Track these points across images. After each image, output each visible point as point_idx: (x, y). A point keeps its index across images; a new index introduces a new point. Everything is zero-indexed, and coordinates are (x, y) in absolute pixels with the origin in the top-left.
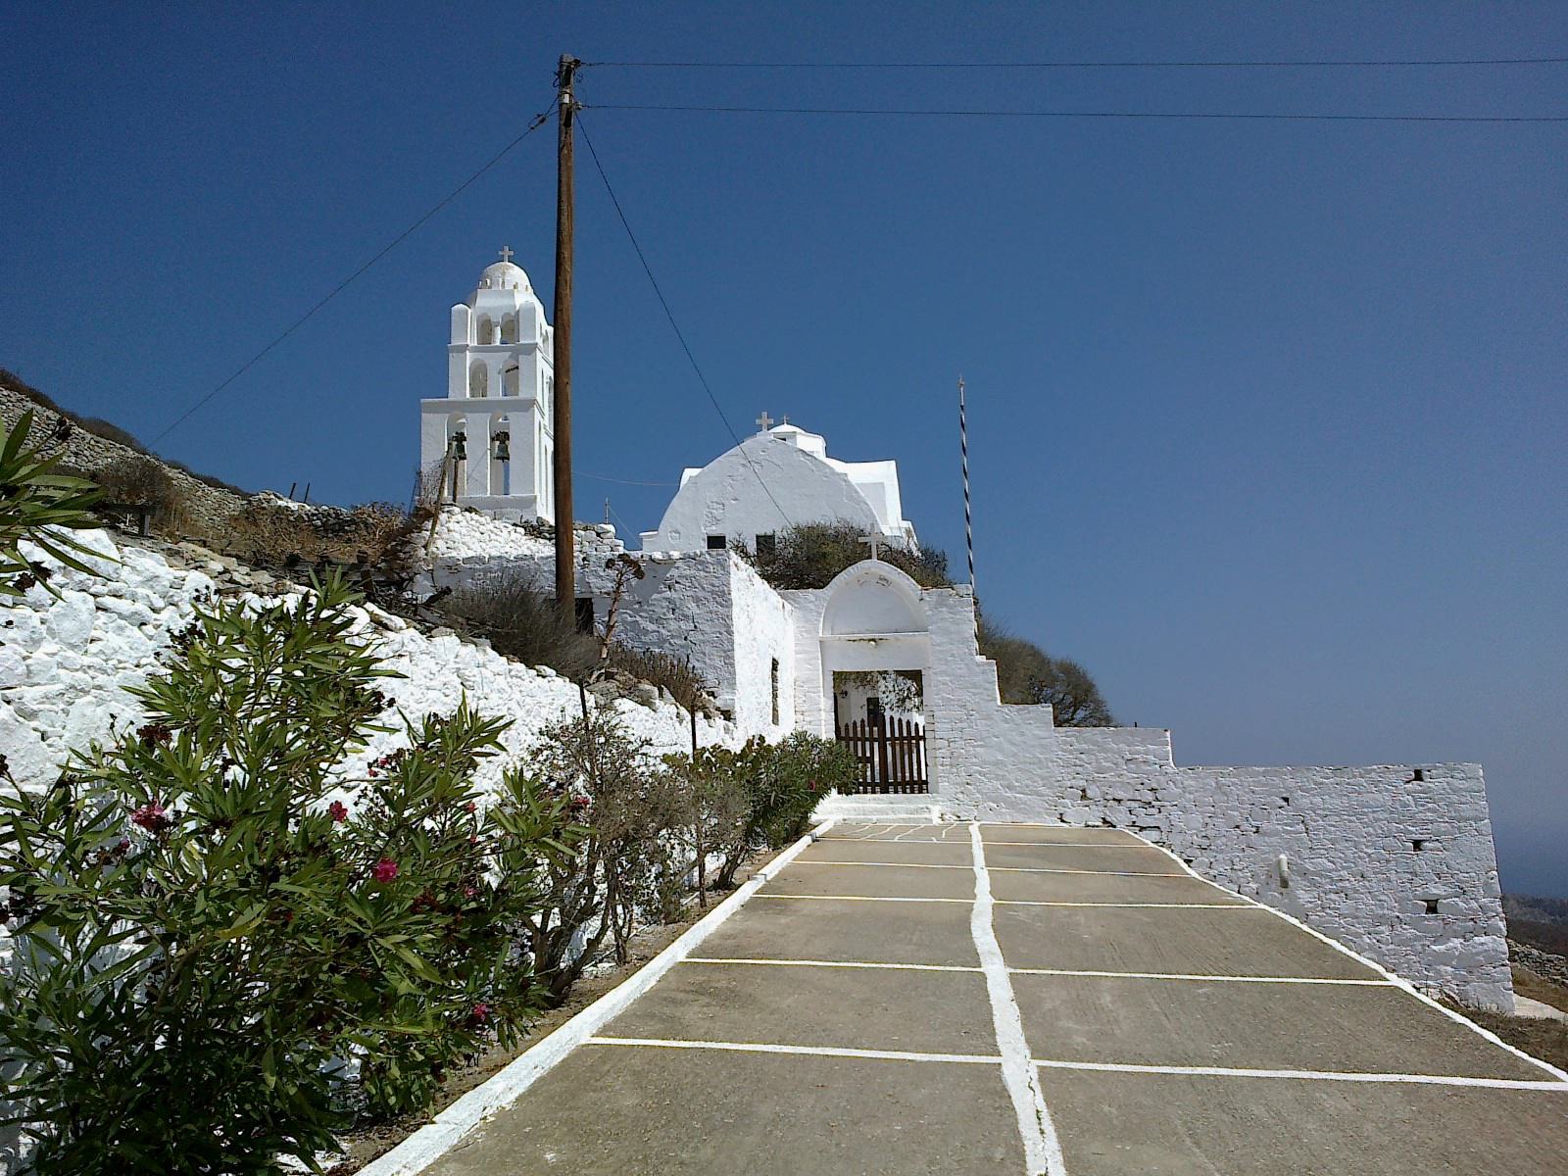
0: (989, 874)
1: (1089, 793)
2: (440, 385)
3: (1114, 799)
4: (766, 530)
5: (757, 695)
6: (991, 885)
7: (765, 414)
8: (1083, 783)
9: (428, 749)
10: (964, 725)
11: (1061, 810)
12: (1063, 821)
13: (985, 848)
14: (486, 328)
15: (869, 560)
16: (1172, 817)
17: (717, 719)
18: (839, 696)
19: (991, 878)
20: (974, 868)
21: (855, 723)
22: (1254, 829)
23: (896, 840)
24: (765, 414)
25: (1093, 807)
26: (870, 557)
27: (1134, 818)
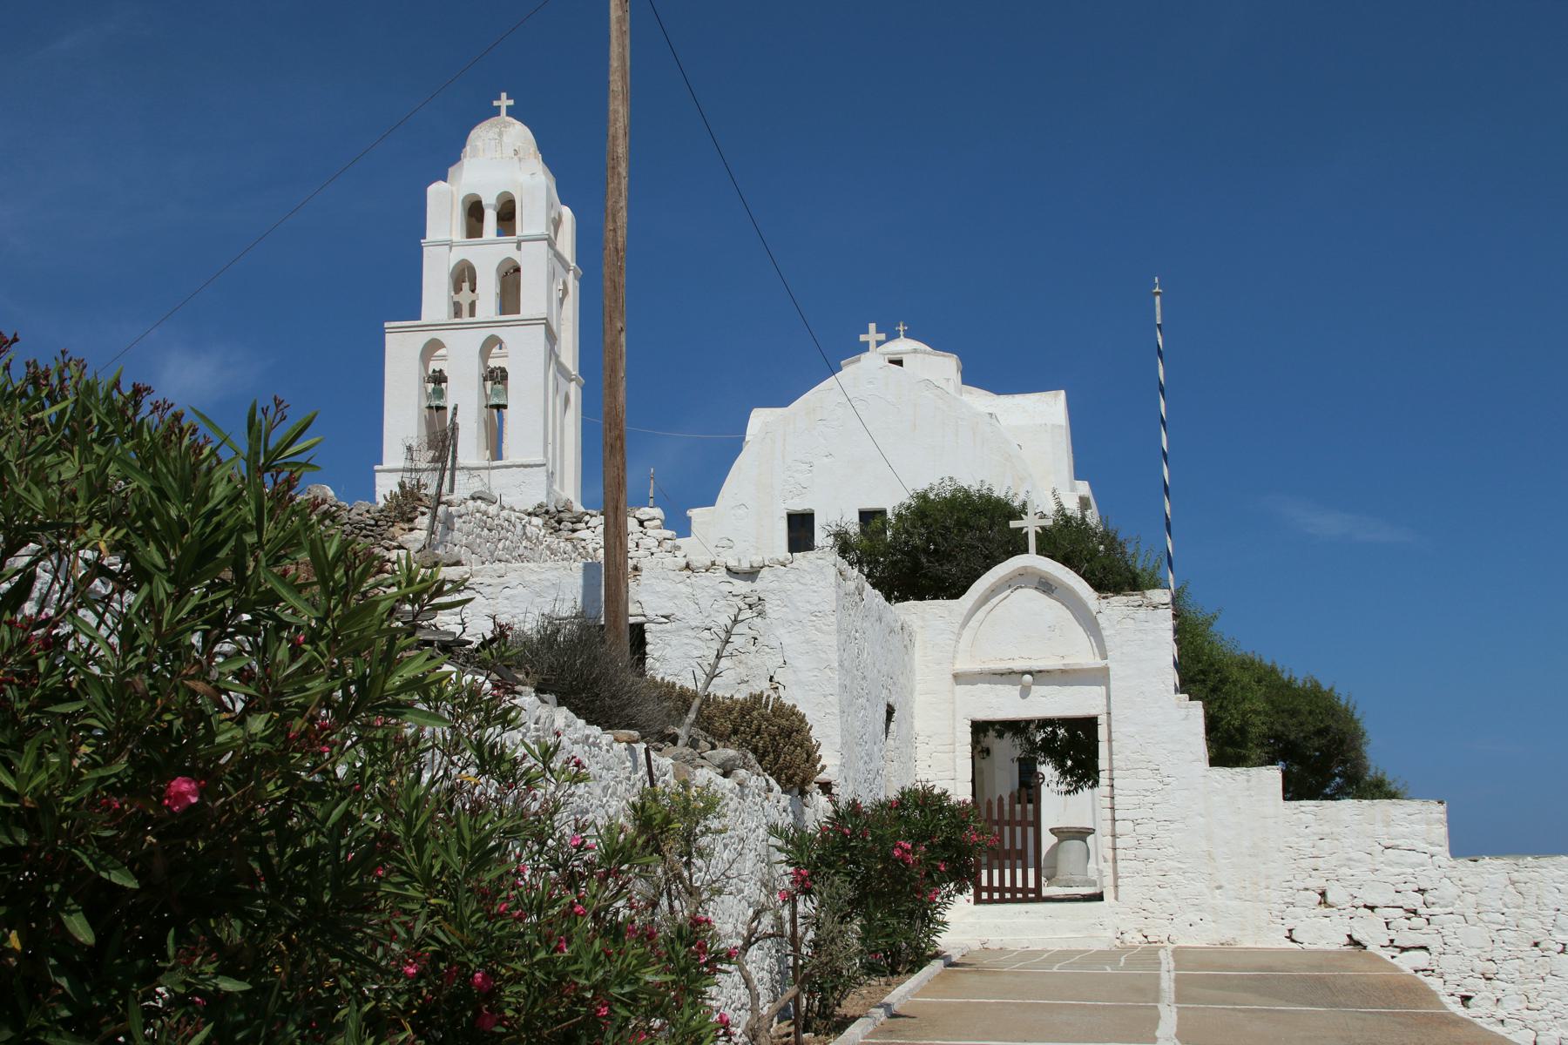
0: (1178, 1013)
1: (1330, 898)
2: (410, 307)
3: (1365, 906)
4: (871, 504)
5: (866, 758)
6: (1178, 1026)
7: (872, 327)
8: (1322, 883)
9: (128, 699)
10: (1157, 798)
11: (1290, 923)
12: (1293, 941)
13: (1178, 980)
14: (474, 211)
15: (982, 716)
16: (1444, 932)
17: (814, 794)
18: (980, 751)
19: (1179, 1018)
20: (1159, 1006)
21: (1001, 799)
22: (1560, 947)
23: (1055, 970)
24: (872, 327)
25: (1336, 918)
26: (1026, 551)
27: (1393, 934)
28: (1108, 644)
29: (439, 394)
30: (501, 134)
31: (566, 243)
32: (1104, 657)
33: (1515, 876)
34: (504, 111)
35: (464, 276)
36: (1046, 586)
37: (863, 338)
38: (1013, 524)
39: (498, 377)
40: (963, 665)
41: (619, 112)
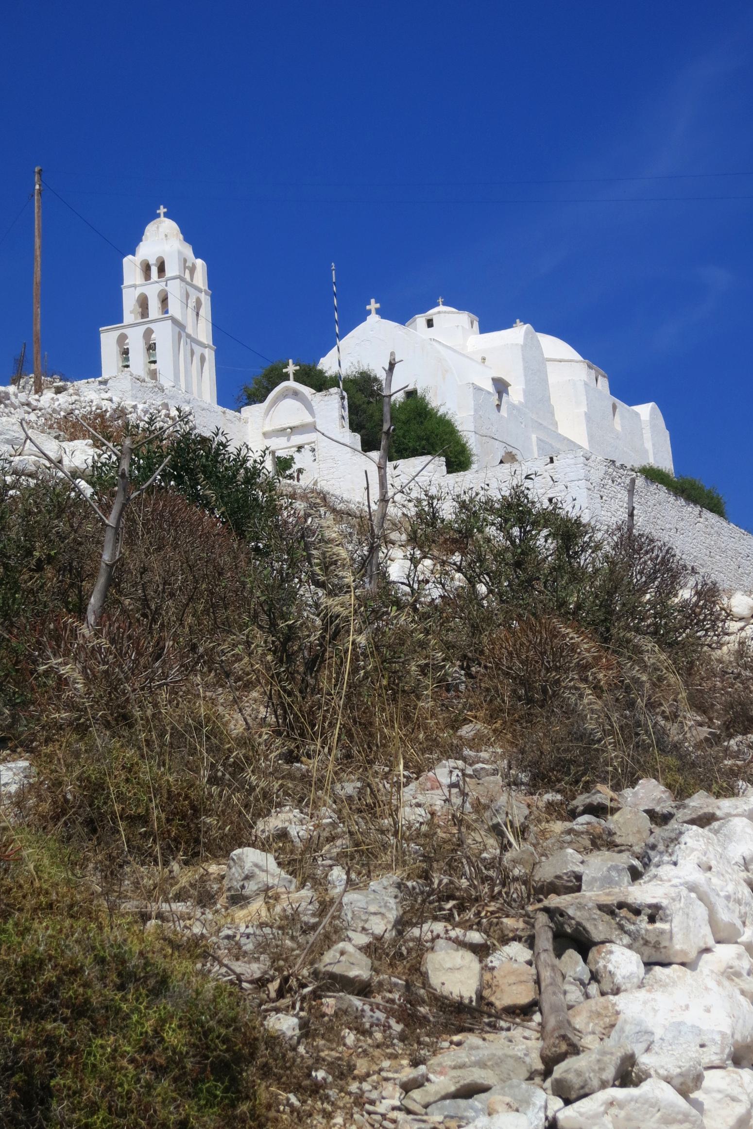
28: (316, 412)
29: (127, 359)
30: (158, 228)
31: (200, 278)
32: (314, 417)
33: (457, 480)
34: (162, 215)
35: (143, 303)
36: (296, 394)
37: (368, 307)
38: (284, 371)
39: (151, 347)
40: (267, 428)
41: (38, 241)
